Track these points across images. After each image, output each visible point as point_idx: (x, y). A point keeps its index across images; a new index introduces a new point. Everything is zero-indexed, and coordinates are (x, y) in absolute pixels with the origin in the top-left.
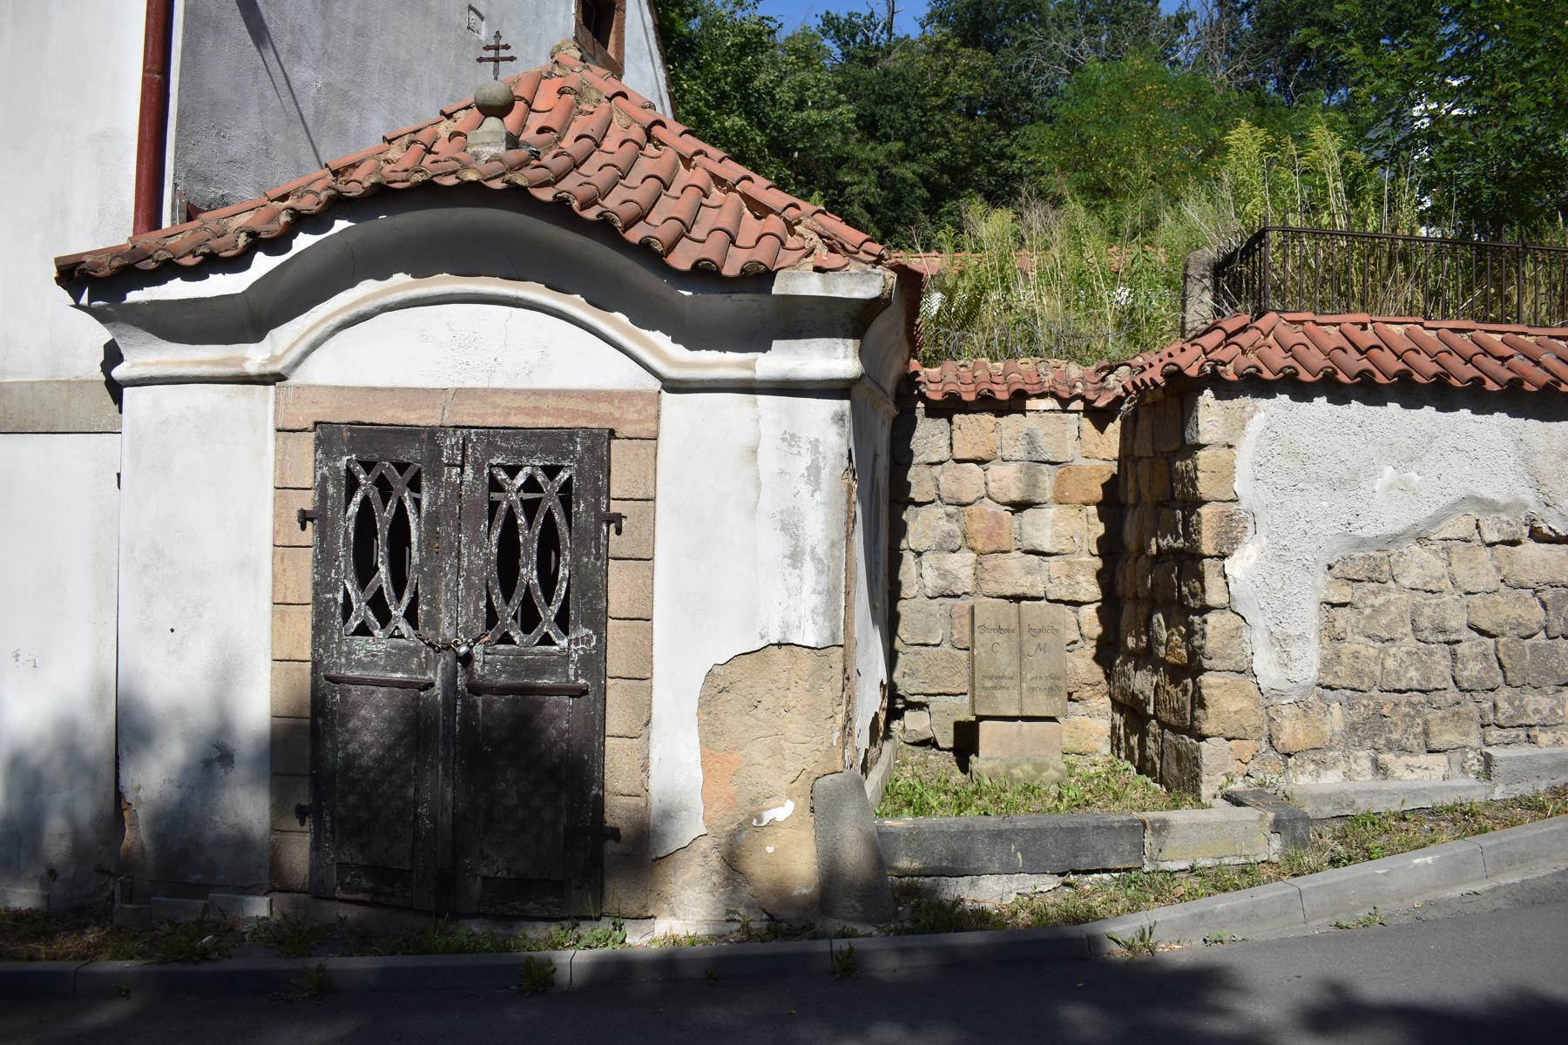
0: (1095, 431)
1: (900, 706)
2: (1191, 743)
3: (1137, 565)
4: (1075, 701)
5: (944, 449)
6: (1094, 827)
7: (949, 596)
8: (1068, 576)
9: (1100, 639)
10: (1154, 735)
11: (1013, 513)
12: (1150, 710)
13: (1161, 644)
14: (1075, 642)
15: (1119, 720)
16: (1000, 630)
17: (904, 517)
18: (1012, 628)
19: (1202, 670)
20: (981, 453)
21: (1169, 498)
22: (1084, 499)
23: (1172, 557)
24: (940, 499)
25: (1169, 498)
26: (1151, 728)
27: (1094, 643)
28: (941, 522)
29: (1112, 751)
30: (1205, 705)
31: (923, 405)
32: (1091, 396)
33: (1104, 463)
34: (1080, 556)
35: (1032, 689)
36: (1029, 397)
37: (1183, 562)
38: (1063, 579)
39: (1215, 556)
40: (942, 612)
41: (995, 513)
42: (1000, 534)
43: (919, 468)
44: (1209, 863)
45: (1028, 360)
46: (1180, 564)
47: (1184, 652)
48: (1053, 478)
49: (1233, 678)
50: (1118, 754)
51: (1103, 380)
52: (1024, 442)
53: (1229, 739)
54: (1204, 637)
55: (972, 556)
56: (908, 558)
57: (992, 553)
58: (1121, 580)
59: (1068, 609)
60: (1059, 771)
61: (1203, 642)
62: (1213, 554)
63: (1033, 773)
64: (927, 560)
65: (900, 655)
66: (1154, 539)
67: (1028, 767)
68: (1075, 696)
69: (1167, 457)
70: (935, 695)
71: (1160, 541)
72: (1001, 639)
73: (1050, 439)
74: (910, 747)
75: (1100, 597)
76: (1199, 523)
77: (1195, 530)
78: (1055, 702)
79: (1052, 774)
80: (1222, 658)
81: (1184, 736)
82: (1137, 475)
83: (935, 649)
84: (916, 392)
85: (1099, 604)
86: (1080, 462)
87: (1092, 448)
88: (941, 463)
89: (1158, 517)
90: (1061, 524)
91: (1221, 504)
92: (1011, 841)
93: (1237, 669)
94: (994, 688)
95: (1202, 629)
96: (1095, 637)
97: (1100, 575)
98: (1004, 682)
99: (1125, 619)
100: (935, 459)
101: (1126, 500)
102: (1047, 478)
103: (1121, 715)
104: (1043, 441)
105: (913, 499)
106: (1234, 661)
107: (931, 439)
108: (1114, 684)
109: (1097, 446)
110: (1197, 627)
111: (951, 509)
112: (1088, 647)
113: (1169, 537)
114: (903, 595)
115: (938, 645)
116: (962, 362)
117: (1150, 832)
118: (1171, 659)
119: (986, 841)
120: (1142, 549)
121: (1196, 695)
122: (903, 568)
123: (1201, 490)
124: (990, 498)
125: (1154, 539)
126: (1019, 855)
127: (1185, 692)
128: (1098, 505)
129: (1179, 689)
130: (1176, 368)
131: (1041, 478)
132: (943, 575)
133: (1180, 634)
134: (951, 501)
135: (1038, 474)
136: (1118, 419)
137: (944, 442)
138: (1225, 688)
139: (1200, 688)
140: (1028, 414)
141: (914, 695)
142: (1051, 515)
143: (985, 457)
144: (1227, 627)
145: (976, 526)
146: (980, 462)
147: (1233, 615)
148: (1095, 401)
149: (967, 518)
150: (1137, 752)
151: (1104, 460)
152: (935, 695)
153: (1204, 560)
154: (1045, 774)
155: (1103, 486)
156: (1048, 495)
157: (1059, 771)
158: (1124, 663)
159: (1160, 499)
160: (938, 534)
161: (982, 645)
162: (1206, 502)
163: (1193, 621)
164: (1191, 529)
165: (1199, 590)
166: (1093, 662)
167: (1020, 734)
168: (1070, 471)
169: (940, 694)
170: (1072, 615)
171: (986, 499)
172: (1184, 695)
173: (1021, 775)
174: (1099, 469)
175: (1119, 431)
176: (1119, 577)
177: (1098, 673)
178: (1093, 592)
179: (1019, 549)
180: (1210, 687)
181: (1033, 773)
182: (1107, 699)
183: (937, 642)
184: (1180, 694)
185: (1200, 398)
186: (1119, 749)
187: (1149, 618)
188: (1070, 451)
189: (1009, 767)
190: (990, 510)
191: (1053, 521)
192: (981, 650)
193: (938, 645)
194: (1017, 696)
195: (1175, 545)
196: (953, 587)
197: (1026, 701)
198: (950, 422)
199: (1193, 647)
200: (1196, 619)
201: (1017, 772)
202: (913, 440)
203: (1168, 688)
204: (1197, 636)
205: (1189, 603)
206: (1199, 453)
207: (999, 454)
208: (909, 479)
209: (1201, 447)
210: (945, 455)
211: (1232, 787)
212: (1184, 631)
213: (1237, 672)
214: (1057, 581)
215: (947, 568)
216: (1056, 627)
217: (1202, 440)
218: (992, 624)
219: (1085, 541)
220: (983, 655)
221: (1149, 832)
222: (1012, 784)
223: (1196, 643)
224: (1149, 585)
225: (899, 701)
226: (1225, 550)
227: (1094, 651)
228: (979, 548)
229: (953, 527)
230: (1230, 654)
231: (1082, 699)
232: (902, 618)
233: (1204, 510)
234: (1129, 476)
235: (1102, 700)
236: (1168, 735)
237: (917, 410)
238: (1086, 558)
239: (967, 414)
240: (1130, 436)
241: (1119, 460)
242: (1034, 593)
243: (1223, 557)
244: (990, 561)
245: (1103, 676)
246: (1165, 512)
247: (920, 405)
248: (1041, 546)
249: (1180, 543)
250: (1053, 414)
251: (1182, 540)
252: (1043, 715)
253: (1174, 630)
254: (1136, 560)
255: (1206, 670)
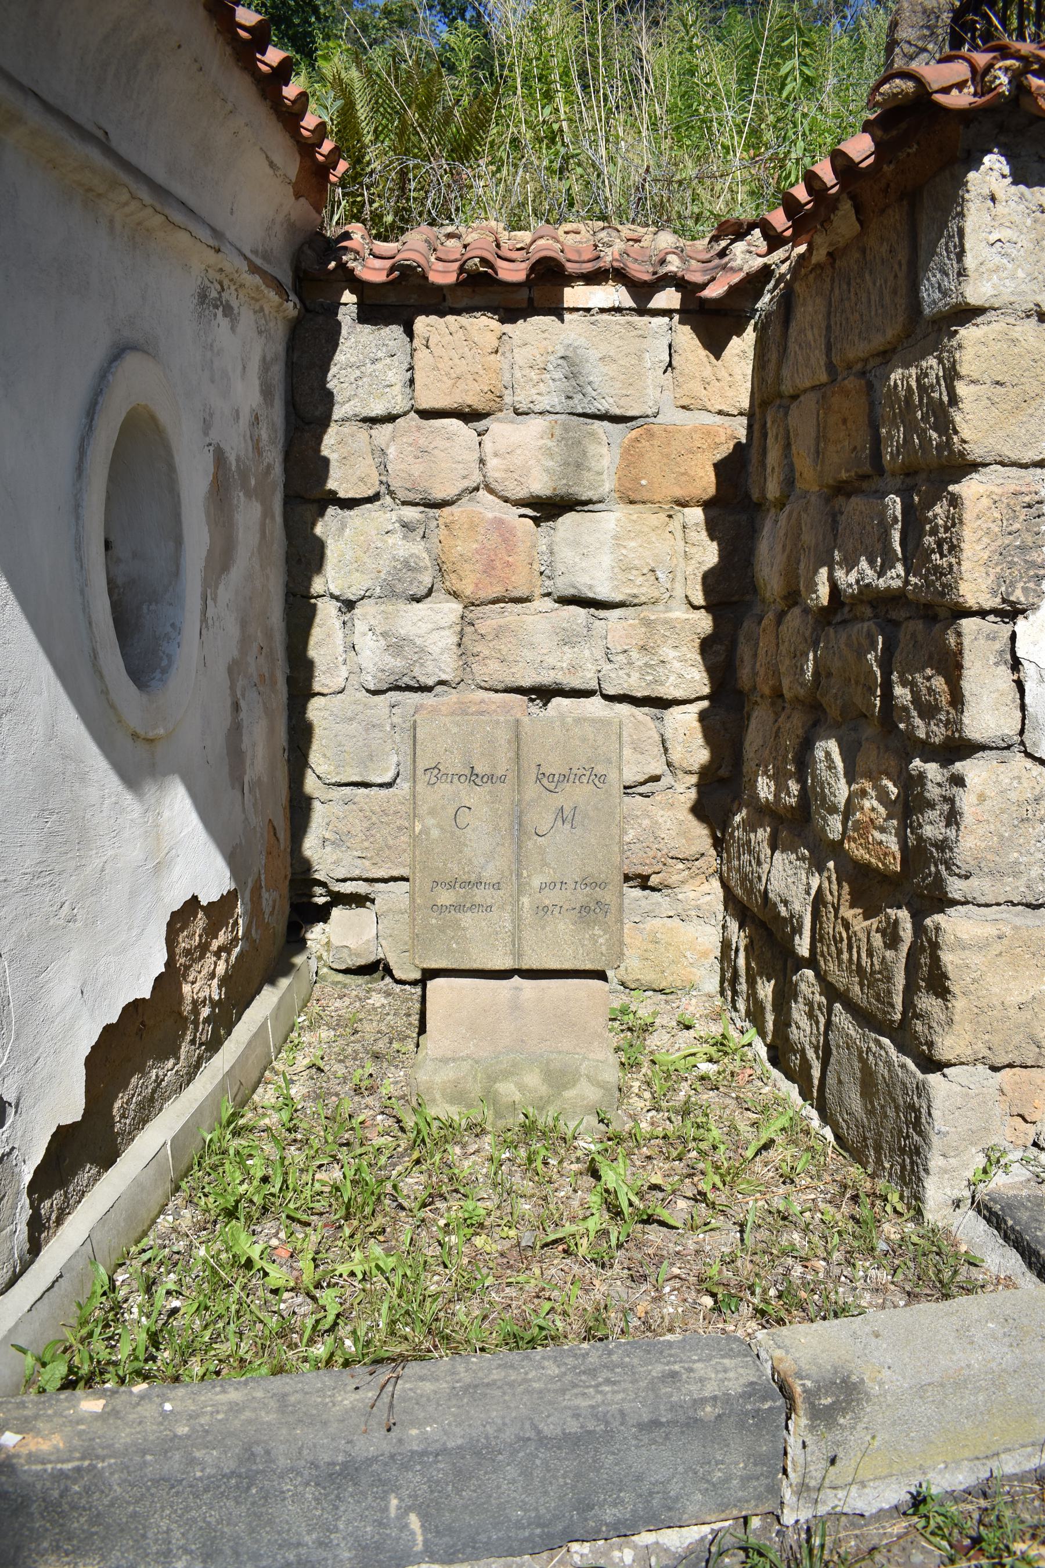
0: (703, 353)
1: (321, 900)
2: (903, 1066)
3: (783, 628)
4: (653, 889)
5: (397, 388)
6: (641, 1427)
7: (409, 688)
8: (643, 648)
9: (704, 773)
10: (810, 1004)
11: (537, 521)
12: (803, 947)
13: (833, 810)
14: (656, 779)
15: (738, 937)
16: (473, 776)
17: (319, 530)
18: (500, 772)
19: (943, 903)
20: (471, 397)
21: (867, 469)
22: (679, 493)
23: (868, 612)
24: (391, 493)
25: (867, 469)
26: (803, 986)
27: (694, 779)
28: (391, 540)
29: (722, 993)
30: (947, 991)
31: (354, 298)
32: (696, 277)
33: (719, 419)
34: (668, 609)
35: (543, 910)
36: (570, 280)
37: (896, 624)
38: (634, 654)
39: (994, 612)
40: (395, 720)
41: (499, 523)
42: (509, 565)
43: (348, 429)
44: (962, 1479)
45: (581, 227)
46: (890, 628)
47: (892, 843)
48: (617, 451)
49: (1018, 921)
50: (734, 1001)
51: (722, 254)
52: (558, 375)
53: (995, 1069)
54: (953, 818)
55: (453, 609)
56: (327, 612)
57: (494, 602)
58: (747, 657)
59: (642, 714)
60: (600, 1085)
61: (951, 833)
62: (987, 605)
63: (544, 1090)
64: (364, 616)
65: (316, 804)
66: (824, 572)
67: (533, 1079)
68: (654, 881)
69: (863, 374)
70: (385, 881)
71: (840, 574)
72: (475, 796)
73: (611, 370)
74: (340, 977)
75: (706, 690)
76: (954, 522)
77: (940, 543)
78: (594, 939)
79: (587, 1092)
80: (996, 874)
81: (886, 1041)
82: (788, 437)
83: (384, 792)
84: (332, 265)
85: (705, 704)
86: (671, 416)
87: (696, 387)
88: (391, 418)
89: (835, 522)
90: (633, 544)
91: (1014, 471)
92: (387, 1486)
93: (1031, 899)
94: (459, 908)
95: (950, 800)
96: (696, 767)
97: (706, 646)
98: (480, 895)
99: (754, 738)
100: (378, 409)
101: (763, 490)
102: (604, 450)
103: (741, 927)
104: (596, 373)
105: (334, 493)
106: (1022, 882)
107: (369, 368)
108: (729, 861)
109: (706, 384)
110: (933, 792)
111: (412, 514)
112: (680, 788)
113: (864, 564)
114: (317, 687)
115: (389, 785)
116: (450, 229)
117: (804, 1421)
118: (859, 853)
119: (309, 1493)
120: (793, 597)
121: (924, 960)
122: (317, 633)
123: (966, 431)
124: (491, 491)
125: (824, 572)
126: (414, 1521)
127: (892, 940)
128: (707, 505)
129: (874, 922)
130: (909, 86)
131: (592, 449)
132: (397, 645)
133: (883, 796)
134: (411, 496)
135: (586, 442)
136: (750, 329)
137: (396, 376)
138: (997, 947)
139: (935, 946)
140: (567, 316)
141: (344, 880)
142: (612, 525)
143: (480, 405)
144: (1013, 796)
145: (462, 547)
146: (470, 416)
147: (1029, 763)
148: (704, 286)
149: (443, 531)
150: (770, 1018)
151: (720, 413)
152: (385, 881)
153: (964, 622)
154: (569, 1094)
155: (717, 466)
156: (607, 485)
157: (600, 1085)
158: (751, 826)
159: (844, 475)
160: (385, 565)
161: (432, 812)
162: (974, 466)
163: (922, 776)
164: (929, 540)
165: (944, 700)
166: (691, 817)
167: (515, 1006)
168: (651, 435)
169: (395, 879)
170: (651, 724)
171: (482, 493)
172: (888, 946)
173: (517, 1097)
174: (708, 432)
175: (751, 354)
176: (744, 650)
177: (700, 836)
178: (693, 680)
179: (548, 594)
180: (962, 946)
181: (544, 1090)
182: (716, 884)
183: (387, 778)
184: (877, 940)
185: (972, 176)
186: (735, 993)
187: (806, 747)
188: (652, 393)
189: (492, 1079)
190: (490, 515)
191: (616, 537)
192: (430, 821)
193: (389, 785)
194: (508, 926)
195: (882, 583)
196: (417, 671)
197: (528, 935)
198: (410, 333)
199: (920, 838)
200: (932, 770)
201: (508, 1090)
202: (333, 370)
203: (847, 913)
204: (932, 815)
205: (912, 728)
206: (963, 332)
207: (508, 399)
208: (325, 452)
209: (968, 314)
210: (396, 400)
211: (999, 1182)
212: (893, 791)
213: (1028, 905)
214: (621, 658)
215: (403, 632)
216: (600, 769)
217: (975, 292)
218: (454, 764)
219: (680, 577)
220: (435, 833)
221: (800, 1422)
222: (498, 1115)
223: (929, 831)
224: (809, 675)
225: (318, 890)
226: (1018, 595)
227: (693, 794)
228: (468, 592)
229: (416, 549)
230: (1016, 863)
231: (667, 887)
232: (318, 732)
233: (969, 488)
234: (770, 441)
235: (706, 888)
236: (841, 1017)
237: (342, 310)
238: (680, 613)
239: (442, 314)
240: (773, 356)
241: (750, 415)
242: (576, 683)
243: (1011, 612)
244: (491, 619)
245: (710, 841)
246: (856, 505)
247: (348, 297)
248: (591, 587)
249: (894, 578)
250: (618, 318)
251: (900, 569)
252: (567, 966)
253: (868, 785)
254: (780, 617)
255: (954, 903)
